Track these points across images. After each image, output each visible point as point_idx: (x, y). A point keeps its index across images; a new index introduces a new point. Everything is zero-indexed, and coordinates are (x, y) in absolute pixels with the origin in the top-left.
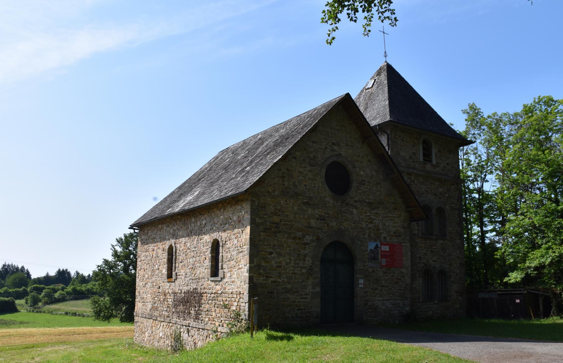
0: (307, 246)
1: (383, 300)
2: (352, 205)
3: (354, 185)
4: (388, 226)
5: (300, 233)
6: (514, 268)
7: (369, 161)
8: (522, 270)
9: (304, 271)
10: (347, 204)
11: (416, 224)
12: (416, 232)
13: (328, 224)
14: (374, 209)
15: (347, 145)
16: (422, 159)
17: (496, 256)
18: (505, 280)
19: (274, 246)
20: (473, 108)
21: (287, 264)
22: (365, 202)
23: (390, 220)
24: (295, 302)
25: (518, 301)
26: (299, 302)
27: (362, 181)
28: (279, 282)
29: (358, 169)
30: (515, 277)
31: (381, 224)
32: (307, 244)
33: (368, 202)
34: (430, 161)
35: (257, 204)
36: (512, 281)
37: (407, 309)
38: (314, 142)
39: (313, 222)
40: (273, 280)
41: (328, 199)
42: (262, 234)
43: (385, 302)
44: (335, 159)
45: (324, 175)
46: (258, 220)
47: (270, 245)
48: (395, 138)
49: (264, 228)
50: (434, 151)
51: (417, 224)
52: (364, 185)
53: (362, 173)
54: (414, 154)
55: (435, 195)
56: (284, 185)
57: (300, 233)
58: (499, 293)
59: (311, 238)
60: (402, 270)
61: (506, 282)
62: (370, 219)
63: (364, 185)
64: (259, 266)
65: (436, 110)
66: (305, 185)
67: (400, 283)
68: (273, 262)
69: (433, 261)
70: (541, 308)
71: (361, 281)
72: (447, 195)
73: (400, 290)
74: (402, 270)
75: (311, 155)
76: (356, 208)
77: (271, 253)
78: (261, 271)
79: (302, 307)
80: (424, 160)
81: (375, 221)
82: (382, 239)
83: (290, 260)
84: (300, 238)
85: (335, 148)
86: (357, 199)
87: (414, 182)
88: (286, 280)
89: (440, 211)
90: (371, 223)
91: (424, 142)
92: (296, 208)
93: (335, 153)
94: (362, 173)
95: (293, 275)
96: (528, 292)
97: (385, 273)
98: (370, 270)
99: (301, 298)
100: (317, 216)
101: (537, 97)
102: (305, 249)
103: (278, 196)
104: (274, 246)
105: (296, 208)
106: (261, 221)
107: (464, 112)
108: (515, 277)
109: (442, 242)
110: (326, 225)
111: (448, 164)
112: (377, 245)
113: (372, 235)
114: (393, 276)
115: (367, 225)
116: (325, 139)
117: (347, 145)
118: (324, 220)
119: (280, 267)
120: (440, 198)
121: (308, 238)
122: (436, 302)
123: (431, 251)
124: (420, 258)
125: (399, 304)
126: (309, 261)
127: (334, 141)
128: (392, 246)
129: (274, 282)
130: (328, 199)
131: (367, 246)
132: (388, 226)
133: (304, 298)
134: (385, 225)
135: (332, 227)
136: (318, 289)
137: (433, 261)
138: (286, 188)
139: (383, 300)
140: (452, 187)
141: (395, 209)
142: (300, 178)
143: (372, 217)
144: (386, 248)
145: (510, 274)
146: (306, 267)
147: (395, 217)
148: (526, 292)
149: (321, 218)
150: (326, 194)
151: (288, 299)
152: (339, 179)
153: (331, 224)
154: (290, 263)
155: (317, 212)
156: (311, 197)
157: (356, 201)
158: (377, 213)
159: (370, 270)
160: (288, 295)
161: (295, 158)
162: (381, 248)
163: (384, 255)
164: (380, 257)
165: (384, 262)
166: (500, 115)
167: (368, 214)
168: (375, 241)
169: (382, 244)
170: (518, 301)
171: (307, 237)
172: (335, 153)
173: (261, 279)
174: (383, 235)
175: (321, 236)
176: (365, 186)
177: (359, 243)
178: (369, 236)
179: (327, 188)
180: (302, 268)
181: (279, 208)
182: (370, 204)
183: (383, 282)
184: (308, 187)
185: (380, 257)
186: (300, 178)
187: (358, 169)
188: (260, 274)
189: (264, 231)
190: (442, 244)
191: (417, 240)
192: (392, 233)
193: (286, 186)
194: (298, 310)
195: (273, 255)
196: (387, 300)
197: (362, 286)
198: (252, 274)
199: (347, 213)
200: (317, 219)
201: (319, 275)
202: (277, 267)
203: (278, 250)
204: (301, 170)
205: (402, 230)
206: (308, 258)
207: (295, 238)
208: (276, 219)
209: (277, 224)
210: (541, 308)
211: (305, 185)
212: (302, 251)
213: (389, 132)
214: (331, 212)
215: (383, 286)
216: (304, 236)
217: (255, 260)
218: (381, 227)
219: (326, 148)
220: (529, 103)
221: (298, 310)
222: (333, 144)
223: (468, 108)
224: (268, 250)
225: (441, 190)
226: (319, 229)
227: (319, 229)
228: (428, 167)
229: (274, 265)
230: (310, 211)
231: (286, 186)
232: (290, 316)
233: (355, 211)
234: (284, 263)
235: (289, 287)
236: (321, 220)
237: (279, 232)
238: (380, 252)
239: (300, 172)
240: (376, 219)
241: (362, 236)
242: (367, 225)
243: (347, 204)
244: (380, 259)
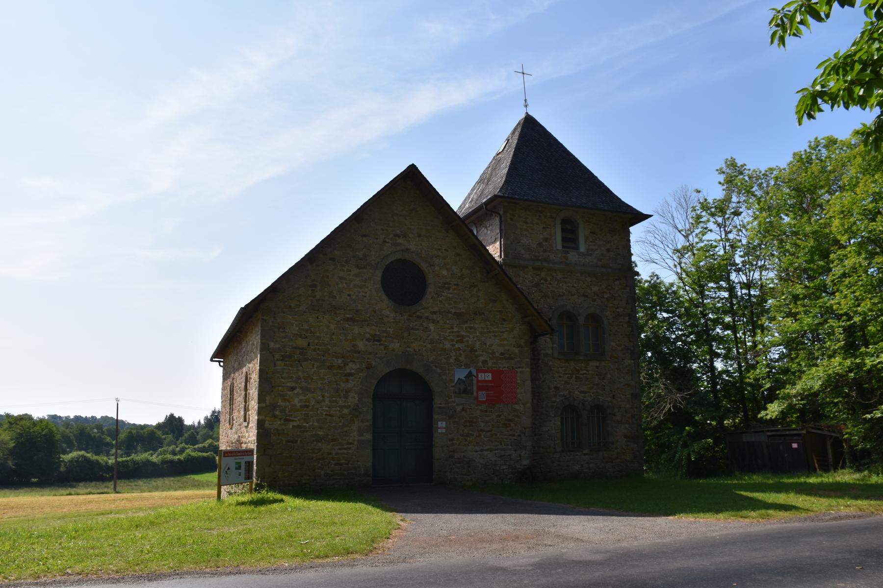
0: (351, 378)
1: (482, 451)
2: (427, 318)
3: (430, 290)
4: (491, 345)
5: (340, 361)
6: (771, 397)
7: (458, 255)
8: (783, 398)
9: (346, 411)
10: (419, 317)
11: (548, 340)
12: (550, 352)
13: (386, 348)
14: (466, 322)
15: (419, 236)
16: (559, 247)
17: (748, 380)
18: (759, 416)
19: (298, 378)
20: (732, 164)
21: (318, 402)
22: (451, 313)
23: (495, 336)
24: (330, 454)
25: (795, 446)
26: (336, 454)
27: (445, 284)
28: (305, 427)
29: (437, 268)
30: (773, 410)
31: (478, 343)
32: (351, 374)
33: (456, 314)
34: (576, 248)
35: (271, 324)
36: (768, 417)
37: (525, 462)
38: (364, 236)
39: (361, 345)
40: (295, 424)
41: (386, 312)
42: (278, 363)
43: (486, 453)
44: (398, 256)
45: (379, 279)
46: (272, 345)
47: (292, 378)
48: (511, 219)
49: (282, 356)
50: (583, 233)
51: (551, 339)
52: (449, 289)
53: (445, 272)
54: (546, 240)
55: (584, 296)
56: (315, 297)
57: (340, 361)
58: (769, 434)
59: (358, 366)
60: (517, 407)
61: (762, 418)
62: (458, 336)
63: (449, 289)
64: (273, 407)
65: (595, 174)
66: (349, 295)
67: (512, 425)
68: (296, 401)
69: (582, 392)
70: (830, 456)
71: (442, 424)
72: (606, 296)
73: (514, 435)
74: (517, 407)
75: (360, 254)
76: (433, 321)
77: (293, 389)
78: (277, 413)
79: (343, 461)
80: (563, 247)
81: (467, 339)
82: (480, 364)
83: (323, 397)
84: (339, 367)
85: (400, 241)
86: (436, 309)
87: (546, 280)
88: (316, 424)
89: (594, 319)
90: (461, 341)
91: (564, 222)
92: (332, 327)
93: (399, 248)
94: (445, 272)
95: (328, 418)
96: (808, 432)
97: (486, 411)
98: (459, 408)
99: (340, 449)
100: (368, 336)
101: (812, 140)
102: (347, 381)
103: (305, 312)
104: (298, 378)
105: (332, 327)
106: (277, 346)
107: (721, 171)
108: (773, 410)
109: (598, 364)
110: (382, 347)
111: (608, 250)
112: (470, 373)
113: (462, 359)
114: (500, 416)
115: (453, 345)
116: (382, 230)
117: (419, 236)
118: (379, 341)
119: (307, 406)
120: (594, 300)
121: (352, 367)
122: (586, 451)
123: (578, 378)
124: (557, 388)
125: (510, 455)
126: (353, 397)
127: (398, 232)
128: (496, 374)
129: (298, 427)
130: (386, 312)
131: (454, 375)
132: (491, 345)
133: (345, 449)
134: (485, 344)
135: (393, 350)
136: (368, 436)
137: (582, 392)
138: (317, 300)
139: (482, 451)
140: (617, 283)
141: (504, 320)
142: (340, 286)
143: (462, 333)
144: (488, 377)
145: (768, 406)
146: (350, 406)
147: (503, 332)
148: (804, 432)
149: (375, 339)
150: (385, 306)
151: (320, 450)
152: (405, 284)
153: (391, 346)
154: (324, 401)
155: (368, 330)
156: (357, 311)
157: (434, 313)
158: (470, 328)
159: (459, 408)
160: (320, 444)
161: (333, 259)
162: (477, 377)
163: (483, 386)
164: (475, 388)
165: (482, 395)
166: (763, 172)
167: (456, 329)
168: (467, 366)
169: (479, 371)
170: (795, 446)
171: (351, 365)
172: (399, 248)
173: (277, 424)
174: (481, 358)
175: (374, 363)
176: (451, 291)
177: (439, 370)
178: (457, 360)
179: (384, 297)
180: (342, 407)
181: (306, 327)
182: (458, 315)
183: (482, 424)
184: (354, 297)
185: (475, 388)
186: (340, 286)
187: (437, 268)
188: (275, 416)
189: (282, 360)
190: (597, 367)
191: (551, 363)
192: (497, 355)
193: (318, 297)
194: (335, 465)
195: (295, 392)
196: (490, 450)
197: (444, 431)
198: (262, 417)
199: (418, 329)
200: (368, 340)
201: (370, 417)
202: (301, 406)
203: (304, 384)
204: (342, 274)
205: (516, 350)
206: (351, 394)
207: (331, 367)
208: (301, 343)
209: (303, 349)
210: (830, 456)
211: (349, 295)
212: (343, 385)
213: (501, 213)
214: (391, 330)
215: (482, 431)
216: (346, 364)
217: (268, 398)
218: (477, 346)
219: (385, 241)
220: (803, 150)
221: (335, 465)
222: (396, 235)
223: (724, 165)
224: (289, 384)
225: (596, 289)
226: (370, 353)
227: (370, 353)
228: (572, 257)
229: (298, 405)
230: (356, 330)
231: (318, 297)
232: (323, 472)
233: (432, 327)
234: (313, 402)
235: (321, 433)
236: (374, 340)
237: (307, 360)
238: (475, 382)
239: (341, 278)
240: (468, 336)
241: (444, 361)
242: (453, 345)
243: (419, 317)
244: (475, 394)
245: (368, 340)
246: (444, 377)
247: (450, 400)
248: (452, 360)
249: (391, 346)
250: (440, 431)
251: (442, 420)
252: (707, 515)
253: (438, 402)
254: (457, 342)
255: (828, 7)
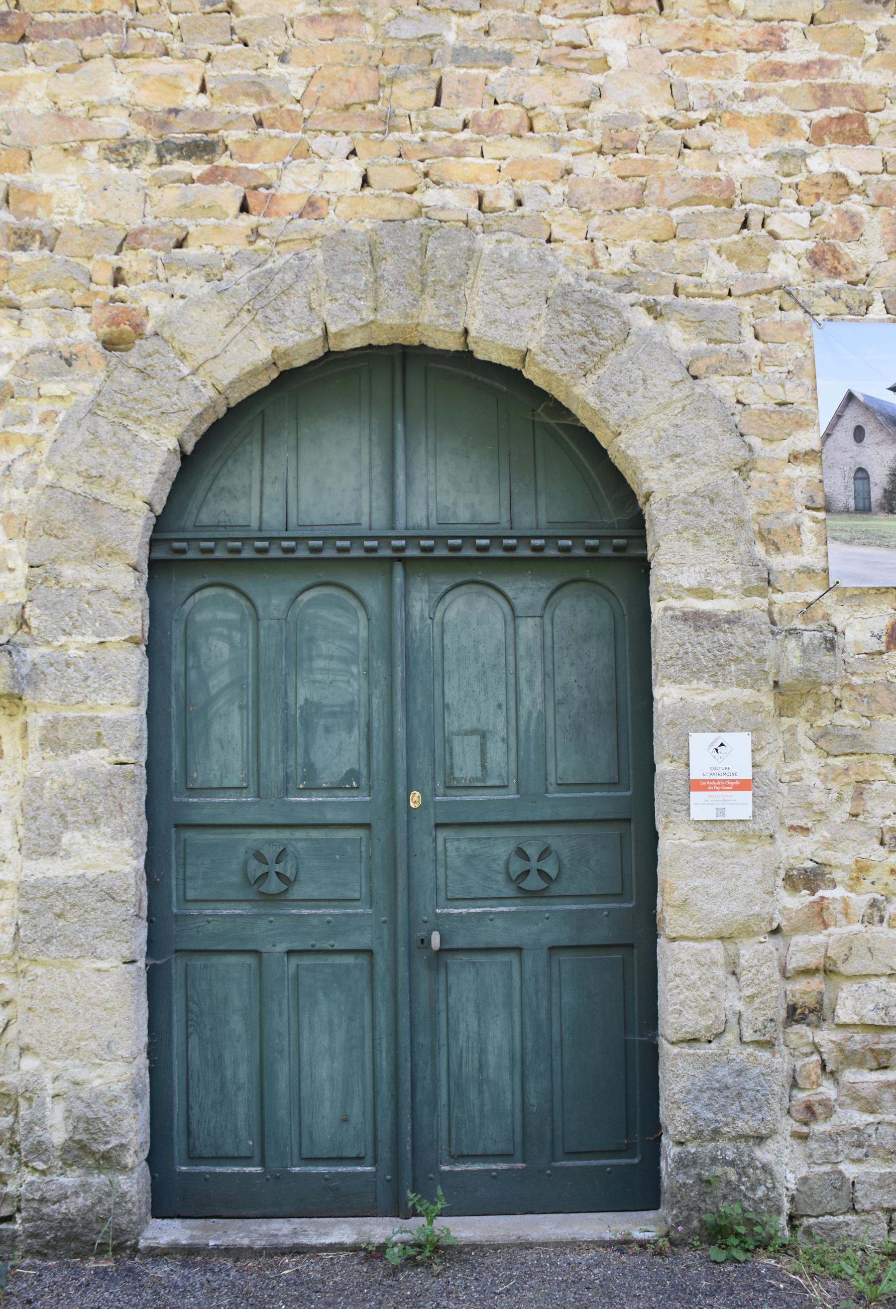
62: (824, 96)
90: (851, 130)
100: (116, 124)
113: (867, 252)
131: (804, 370)
143: (854, 73)
153: (295, 183)
167: (800, 50)
177: (679, 338)
197: (740, 806)
200: (119, 151)
236: (167, 150)
241: (718, 270)
245: (119, 151)
246: (724, 387)
247: (785, 562)
248: (784, 267)
249: (295, 183)
250: (703, 806)
251: (724, 720)
252: (442, 347)
253: (683, 571)
254: (818, 134)
255: (180, 55)
